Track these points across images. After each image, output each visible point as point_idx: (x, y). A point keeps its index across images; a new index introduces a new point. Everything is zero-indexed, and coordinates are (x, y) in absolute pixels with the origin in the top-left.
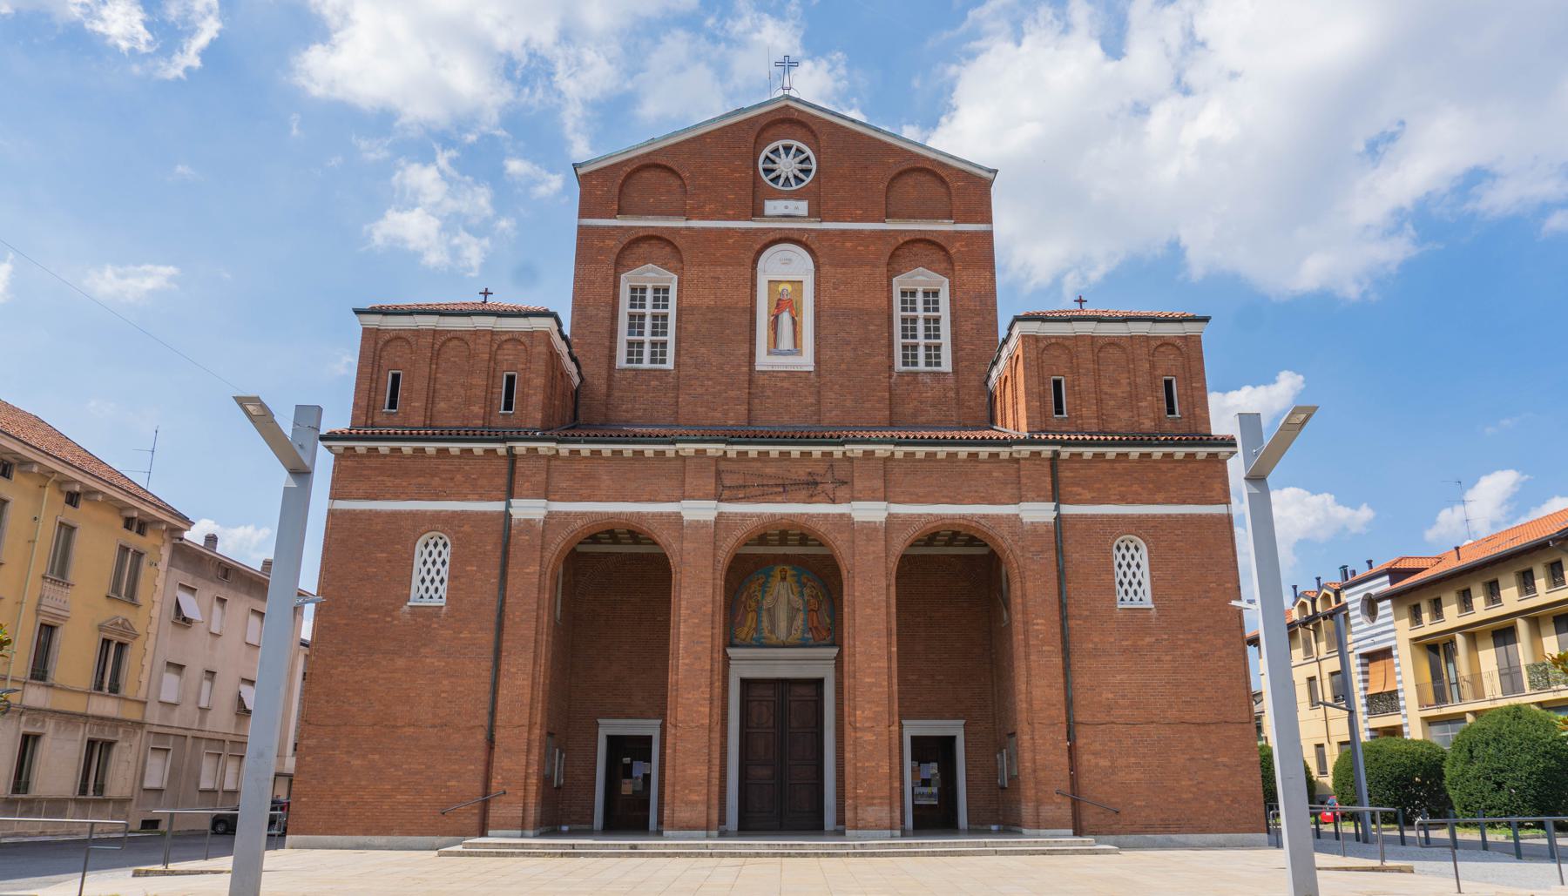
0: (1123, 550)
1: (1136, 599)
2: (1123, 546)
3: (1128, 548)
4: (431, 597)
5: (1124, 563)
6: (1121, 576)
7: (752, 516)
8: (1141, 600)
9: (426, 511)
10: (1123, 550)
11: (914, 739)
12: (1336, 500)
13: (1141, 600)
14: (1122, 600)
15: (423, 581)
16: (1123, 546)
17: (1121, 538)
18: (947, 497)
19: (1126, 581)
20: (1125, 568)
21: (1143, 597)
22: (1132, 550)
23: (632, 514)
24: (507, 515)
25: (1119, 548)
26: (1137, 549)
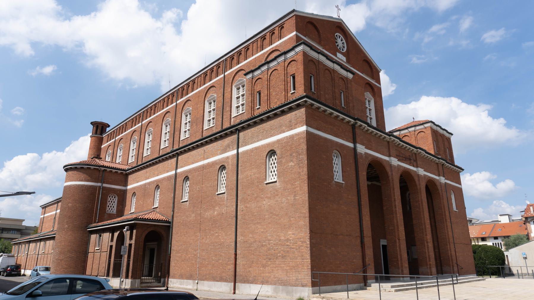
0: (111, 197)
1: (112, 211)
2: (111, 196)
3: (112, 197)
4: (110, 211)
5: (110, 201)
6: (109, 204)
7: (403, 167)
8: (113, 211)
9: (334, 141)
10: (111, 197)
11: (382, 245)
12: (503, 181)
13: (113, 211)
14: (108, 211)
15: (113, 207)
16: (111, 196)
17: (111, 194)
18: (445, 152)
19: (110, 206)
20: (110, 202)
21: (114, 211)
22: (113, 198)
23: (222, 159)
24: (355, 149)
25: (110, 197)
26: (115, 197)
